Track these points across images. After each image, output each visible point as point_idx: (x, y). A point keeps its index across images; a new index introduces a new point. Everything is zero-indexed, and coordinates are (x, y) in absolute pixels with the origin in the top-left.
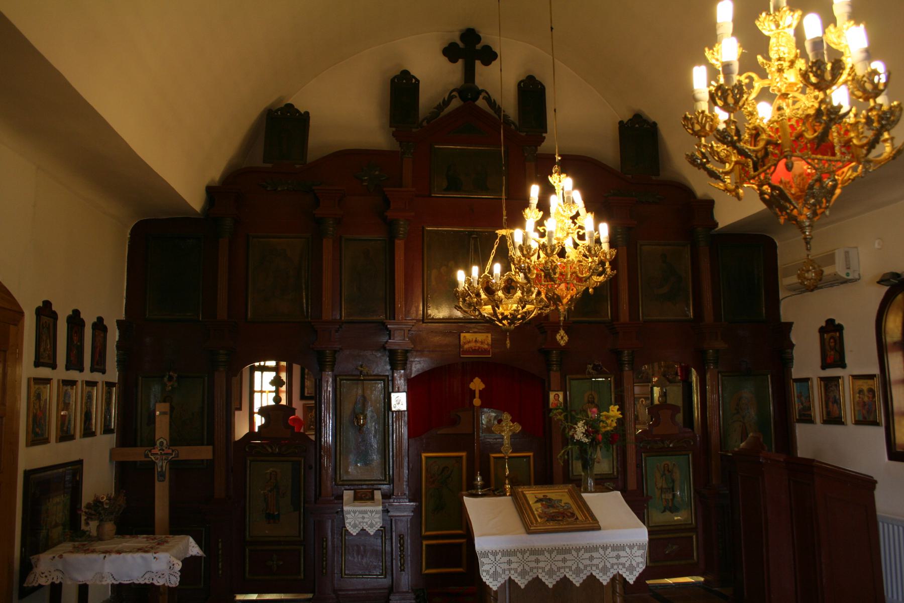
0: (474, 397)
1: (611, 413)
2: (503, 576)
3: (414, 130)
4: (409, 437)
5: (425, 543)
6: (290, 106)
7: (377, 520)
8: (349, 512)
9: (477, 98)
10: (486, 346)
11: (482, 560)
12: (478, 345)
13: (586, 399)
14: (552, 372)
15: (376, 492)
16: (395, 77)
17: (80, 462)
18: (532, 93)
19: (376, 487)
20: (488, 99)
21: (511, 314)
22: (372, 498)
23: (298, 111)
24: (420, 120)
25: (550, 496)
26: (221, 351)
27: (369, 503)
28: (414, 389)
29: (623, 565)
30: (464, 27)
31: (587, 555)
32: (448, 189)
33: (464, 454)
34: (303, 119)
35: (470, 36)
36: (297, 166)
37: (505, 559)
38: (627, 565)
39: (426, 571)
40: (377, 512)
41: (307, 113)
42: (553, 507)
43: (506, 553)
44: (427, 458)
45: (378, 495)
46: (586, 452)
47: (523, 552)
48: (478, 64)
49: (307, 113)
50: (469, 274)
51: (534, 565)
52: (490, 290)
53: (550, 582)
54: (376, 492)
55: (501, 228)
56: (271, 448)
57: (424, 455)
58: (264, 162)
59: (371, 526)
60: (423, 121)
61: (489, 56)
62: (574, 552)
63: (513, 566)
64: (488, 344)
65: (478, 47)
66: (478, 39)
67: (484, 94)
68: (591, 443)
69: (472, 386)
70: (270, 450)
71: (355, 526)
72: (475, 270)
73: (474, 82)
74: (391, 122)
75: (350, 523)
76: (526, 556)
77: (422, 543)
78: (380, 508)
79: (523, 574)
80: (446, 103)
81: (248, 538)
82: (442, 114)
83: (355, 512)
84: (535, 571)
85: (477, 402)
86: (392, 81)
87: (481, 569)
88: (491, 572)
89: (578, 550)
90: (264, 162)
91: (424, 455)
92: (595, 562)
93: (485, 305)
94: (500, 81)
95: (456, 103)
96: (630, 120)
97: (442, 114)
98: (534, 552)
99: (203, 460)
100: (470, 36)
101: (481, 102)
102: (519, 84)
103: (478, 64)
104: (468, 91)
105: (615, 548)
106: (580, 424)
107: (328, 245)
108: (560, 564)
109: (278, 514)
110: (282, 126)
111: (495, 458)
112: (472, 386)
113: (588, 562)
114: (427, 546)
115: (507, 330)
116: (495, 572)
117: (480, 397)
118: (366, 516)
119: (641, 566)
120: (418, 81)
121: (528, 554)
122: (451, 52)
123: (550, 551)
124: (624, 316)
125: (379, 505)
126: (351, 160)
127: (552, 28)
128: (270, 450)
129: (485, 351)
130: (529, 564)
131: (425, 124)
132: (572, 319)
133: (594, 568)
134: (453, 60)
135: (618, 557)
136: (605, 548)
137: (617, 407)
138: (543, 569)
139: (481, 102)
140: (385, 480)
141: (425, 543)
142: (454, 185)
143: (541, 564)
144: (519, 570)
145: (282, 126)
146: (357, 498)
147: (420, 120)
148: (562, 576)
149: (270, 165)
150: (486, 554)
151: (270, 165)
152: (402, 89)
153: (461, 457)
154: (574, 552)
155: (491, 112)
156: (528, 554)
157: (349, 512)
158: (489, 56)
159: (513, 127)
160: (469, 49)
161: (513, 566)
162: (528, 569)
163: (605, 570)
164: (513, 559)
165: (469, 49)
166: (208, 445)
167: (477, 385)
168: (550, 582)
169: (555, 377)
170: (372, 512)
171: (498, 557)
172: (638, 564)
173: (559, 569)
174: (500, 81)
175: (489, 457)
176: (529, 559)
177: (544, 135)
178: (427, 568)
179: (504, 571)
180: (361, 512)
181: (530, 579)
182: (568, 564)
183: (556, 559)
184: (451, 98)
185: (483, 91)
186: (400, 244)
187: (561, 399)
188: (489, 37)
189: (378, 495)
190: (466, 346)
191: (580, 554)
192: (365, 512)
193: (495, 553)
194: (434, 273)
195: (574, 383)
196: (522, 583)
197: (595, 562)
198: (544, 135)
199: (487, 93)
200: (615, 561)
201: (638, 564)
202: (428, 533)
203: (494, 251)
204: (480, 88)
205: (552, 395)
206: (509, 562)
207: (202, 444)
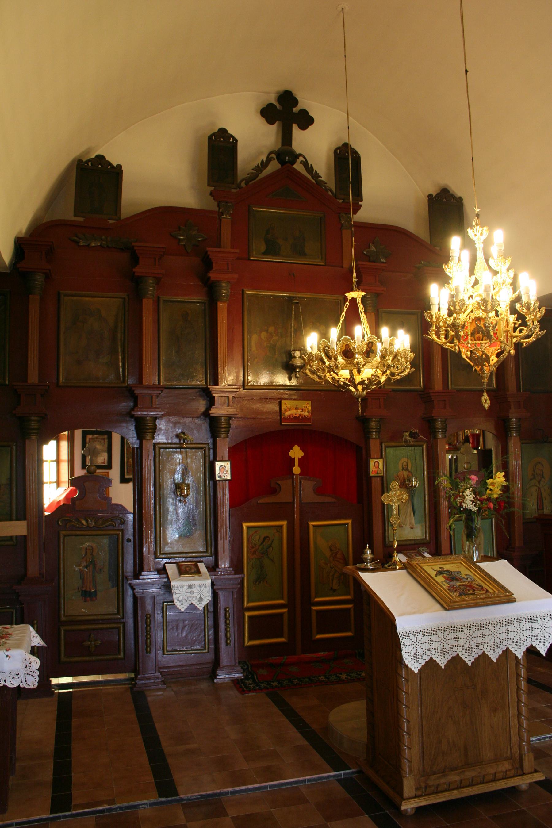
0: (294, 466)
1: (497, 480)
2: (424, 657)
3: (233, 190)
4: (231, 507)
5: (247, 614)
6: (100, 158)
7: (207, 594)
8: (177, 588)
9: (294, 162)
10: (306, 414)
11: (404, 642)
12: (299, 412)
13: (401, 468)
14: (372, 441)
15: (200, 564)
16: (214, 134)
17: (514, 601)
18: (347, 161)
19: (197, 559)
20: (305, 164)
21: (368, 379)
22: (198, 572)
23: (110, 164)
24: (239, 181)
25: (447, 567)
26: (33, 418)
27: (196, 576)
28: (234, 456)
29: (536, 636)
30: (282, 88)
31: (503, 629)
32: (265, 253)
33: (284, 523)
34: (115, 174)
35: (287, 98)
36: (111, 222)
37: (426, 639)
38: (540, 637)
39: (247, 643)
40: (206, 586)
41: (119, 167)
42: (457, 580)
43: (427, 632)
44: (248, 528)
45: (202, 567)
46: (472, 520)
47: (443, 630)
48: (295, 127)
49: (119, 167)
50: (324, 335)
51: (453, 643)
52: (348, 353)
53: (469, 660)
54: (200, 564)
55: (352, 290)
56: (87, 522)
57: (245, 525)
58: (75, 215)
59: (201, 600)
60: (242, 181)
61: (305, 120)
62: (491, 627)
63: (435, 645)
64: (308, 412)
65: (295, 110)
66: (296, 102)
67: (301, 158)
68: (478, 511)
69: (292, 454)
70: (84, 522)
71: (184, 601)
72: (334, 332)
73: (291, 145)
74: (208, 181)
75: (178, 599)
76: (446, 634)
77: (244, 615)
78: (209, 582)
79: (444, 652)
80: (264, 165)
81: (63, 618)
82: (261, 176)
83: (183, 587)
84: (455, 649)
85: (296, 470)
86: (210, 138)
87: (403, 651)
88: (412, 653)
89: (495, 624)
90: (75, 215)
91: (245, 525)
92: (511, 635)
93: (342, 369)
94: (315, 146)
95: (274, 166)
96: (438, 194)
97: (261, 176)
98: (454, 629)
99: (11, 537)
100: (287, 98)
101: (298, 166)
102: (335, 152)
103: (295, 127)
104: (285, 154)
105: (531, 619)
106: (468, 492)
107: (148, 305)
108: (479, 640)
109: (95, 591)
110: (95, 178)
111: (314, 526)
112: (292, 454)
113: (503, 636)
114: (249, 617)
115: (359, 396)
116: (417, 653)
117: (299, 466)
118: (194, 590)
119: (207, 598)
120: (236, 141)
121: (447, 632)
122: (268, 113)
123: (469, 628)
124: (438, 385)
125: (207, 579)
126: (165, 217)
127: (467, 71)
128: (84, 522)
129: (305, 419)
130: (448, 642)
131: (243, 185)
132: (386, 387)
133: (510, 642)
134: (270, 122)
135: (531, 629)
136: (519, 620)
137: (503, 474)
138: (463, 646)
139: (298, 166)
140: (207, 552)
141: (247, 614)
142: (272, 249)
143: (461, 642)
144: (440, 649)
145: (95, 178)
146: (182, 571)
147: (239, 181)
148: (480, 653)
149: (81, 219)
150: (407, 635)
151: (81, 219)
152: (220, 148)
153: (281, 526)
154: (491, 627)
155: (309, 177)
156: (447, 632)
157: (177, 588)
158: (305, 120)
159: (330, 193)
160: (285, 112)
161: (435, 645)
162: (448, 648)
163: (519, 643)
164: (434, 638)
165: (285, 112)
166: (18, 519)
167: (296, 453)
168: (469, 660)
169: (374, 445)
170: (200, 586)
171: (419, 638)
172: (205, 597)
173: (477, 645)
174: (315, 146)
175: (308, 524)
176: (449, 637)
177: (360, 203)
178: (250, 639)
179: (425, 652)
180: (189, 587)
181: (450, 658)
182: (486, 639)
183: (475, 635)
184: (269, 160)
185: (301, 155)
186: (222, 306)
187: (381, 466)
188: (307, 102)
189: (202, 567)
190: (287, 414)
191: (497, 628)
192: (194, 587)
193: (416, 634)
194: (255, 337)
195: (388, 450)
196: (442, 662)
197: (511, 635)
198: (360, 203)
199: (305, 158)
200: (528, 633)
201: (205, 597)
202: (251, 604)
203: (344, 313)
204: (298, 152)
205: (372, 463)
206: (430, 642)
207: (11, 520)
